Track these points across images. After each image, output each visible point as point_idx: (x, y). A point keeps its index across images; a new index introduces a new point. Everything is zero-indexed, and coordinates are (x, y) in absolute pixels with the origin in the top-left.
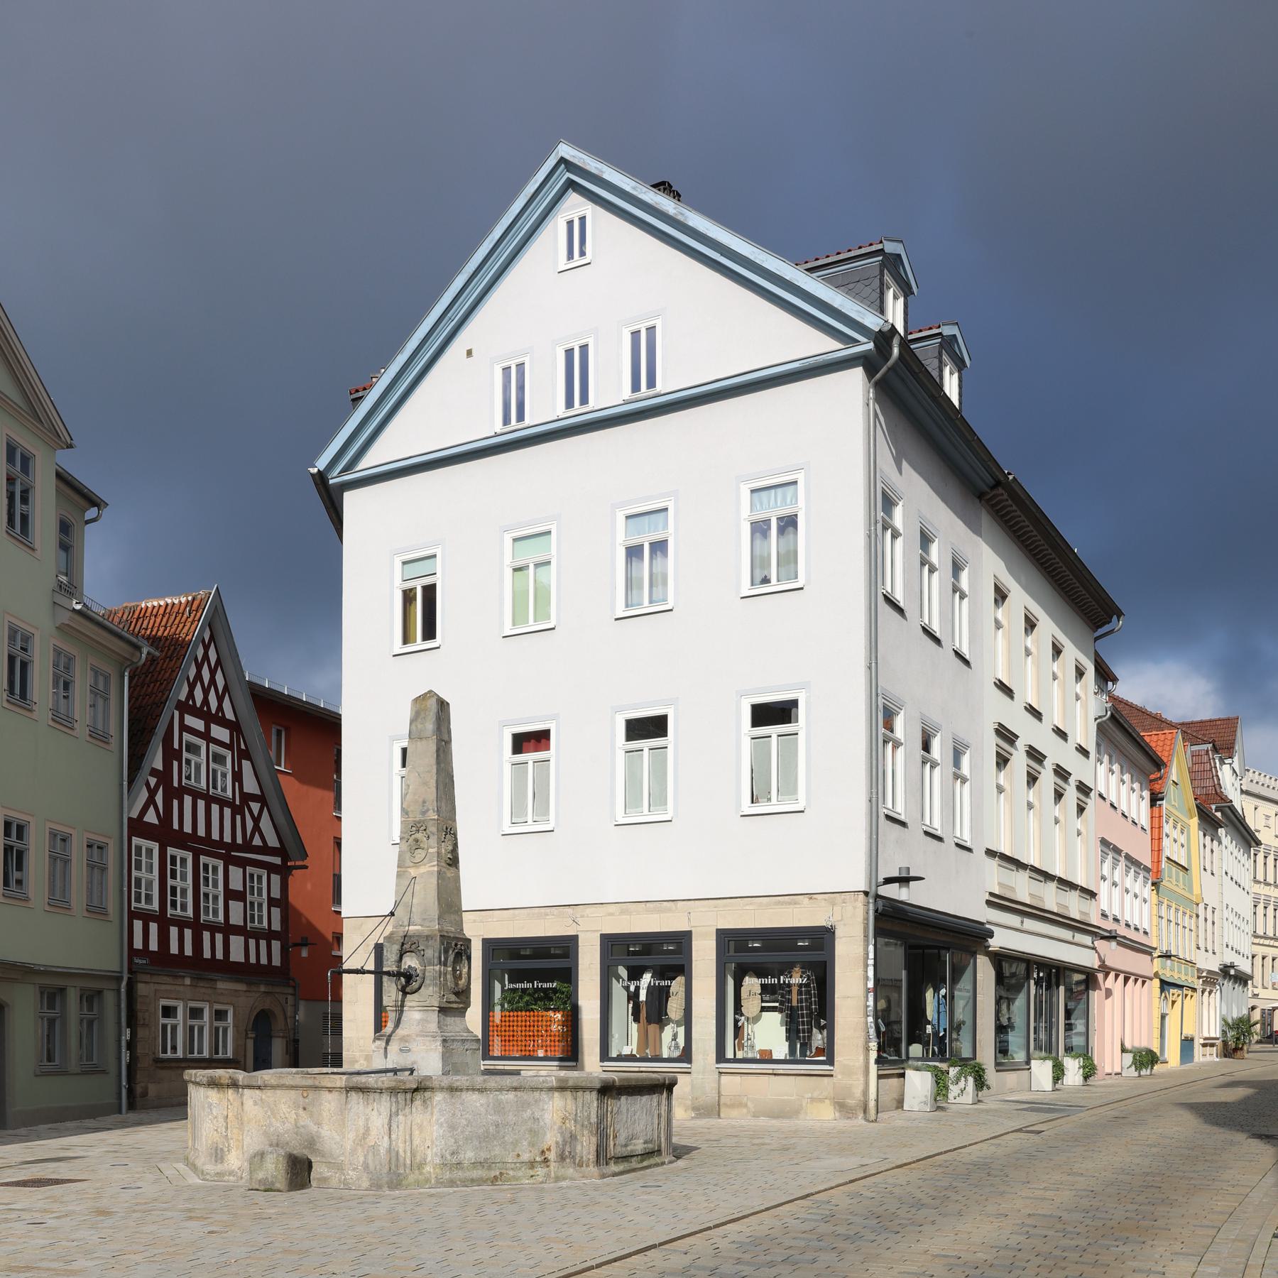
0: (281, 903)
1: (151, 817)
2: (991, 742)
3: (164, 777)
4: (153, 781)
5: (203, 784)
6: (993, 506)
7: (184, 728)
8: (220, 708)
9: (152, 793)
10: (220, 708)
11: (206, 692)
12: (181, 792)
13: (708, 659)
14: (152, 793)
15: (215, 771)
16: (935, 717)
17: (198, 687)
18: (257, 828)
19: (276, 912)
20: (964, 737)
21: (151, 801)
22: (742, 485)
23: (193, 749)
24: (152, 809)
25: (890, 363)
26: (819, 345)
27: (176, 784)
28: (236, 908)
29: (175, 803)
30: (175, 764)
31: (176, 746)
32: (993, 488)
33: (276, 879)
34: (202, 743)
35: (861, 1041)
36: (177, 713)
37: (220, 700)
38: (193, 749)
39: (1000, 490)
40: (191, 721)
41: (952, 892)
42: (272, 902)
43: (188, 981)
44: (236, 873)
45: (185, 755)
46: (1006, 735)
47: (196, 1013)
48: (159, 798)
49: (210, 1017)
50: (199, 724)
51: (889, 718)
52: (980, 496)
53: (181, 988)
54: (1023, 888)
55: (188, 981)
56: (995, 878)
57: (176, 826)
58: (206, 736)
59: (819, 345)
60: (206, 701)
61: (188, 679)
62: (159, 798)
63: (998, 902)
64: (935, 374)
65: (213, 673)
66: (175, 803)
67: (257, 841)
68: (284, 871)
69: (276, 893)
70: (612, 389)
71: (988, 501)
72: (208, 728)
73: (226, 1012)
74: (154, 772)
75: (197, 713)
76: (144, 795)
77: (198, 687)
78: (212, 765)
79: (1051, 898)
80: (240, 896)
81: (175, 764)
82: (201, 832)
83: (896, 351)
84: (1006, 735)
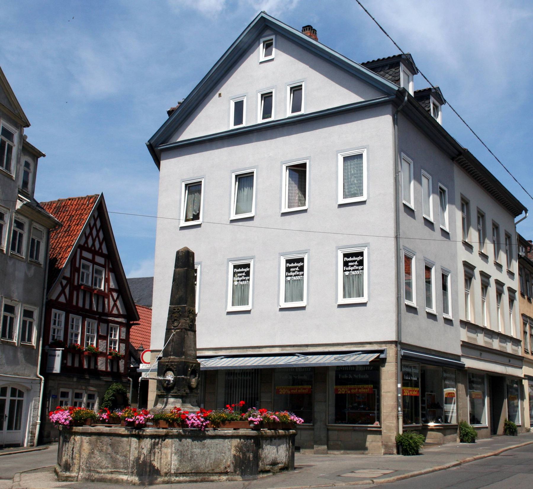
0: (126, 341)
1: (62, 299)
2: (461, 270)
3: (70, 281)
4: (64, 282)
5: (90, 284)
6: (459, 163)
7: (82, 257)
8: (100, 248)
9: (64, 288)
10: (100, 248)
11: (94, 241)
12: (78, 288)
13: (325, 229)
14: (64, 288)
15: (96, 278)
16: (431, 258)
17: (90, 238)
18: (115, 305)
19: (123, 346)
20: (447, 267)
21: (63, 292)
22: (339, 154)
23: (85, 267)
24: (63, 296)
25: (404, 104)
26: (374, 96)
27: (76, 283)
28: (102, 343)
29: (75, 293)
30: (76, 275)
31: (77, 265)
32: (458, 155)
33: (124, 329)
34: (91, 265)
35: (395, 414)
36: (79, 250)
37: (101, 244)
38: (85, 267)
39: (462, 157)
40: (86, 254)
41: (448, 342)
42: (121, 341)
43: (75, 379)
44: (103, 326)
45: (81, 270)
46: (469, 268)
47: (78, 396)
48: (67, 291)
49: (72, 397)
50: (89, 256)
51: (408, 260)
52: (453, 159)
53: (72, 383)
54: (481, 340)
55: (75, 379)
56: (464, 335)
57: (74, 303)
58: (93, 261)
59: (374, 96)
60: (93, 245)
61: (85, 234)
62: (67, 291)
63: (465, 345)
64: (69, 266)
65: (98, 232)
66: (75, 293)
67: (115, 312)
68: (128, 326)
69: (123, 336)
70: (283, 110)
71: (457, 161)
72: (94, 258)
73: (68, 393)
74: (65, 278)
75: (89, 250)
76: (60, 289)
77: (90, 238)
78: (94, 275)
79: (496, 344)
80: (105, 338)
81: (76, 275)
82: (87, 307)
83: (406, 98)
84: (469, 268)
